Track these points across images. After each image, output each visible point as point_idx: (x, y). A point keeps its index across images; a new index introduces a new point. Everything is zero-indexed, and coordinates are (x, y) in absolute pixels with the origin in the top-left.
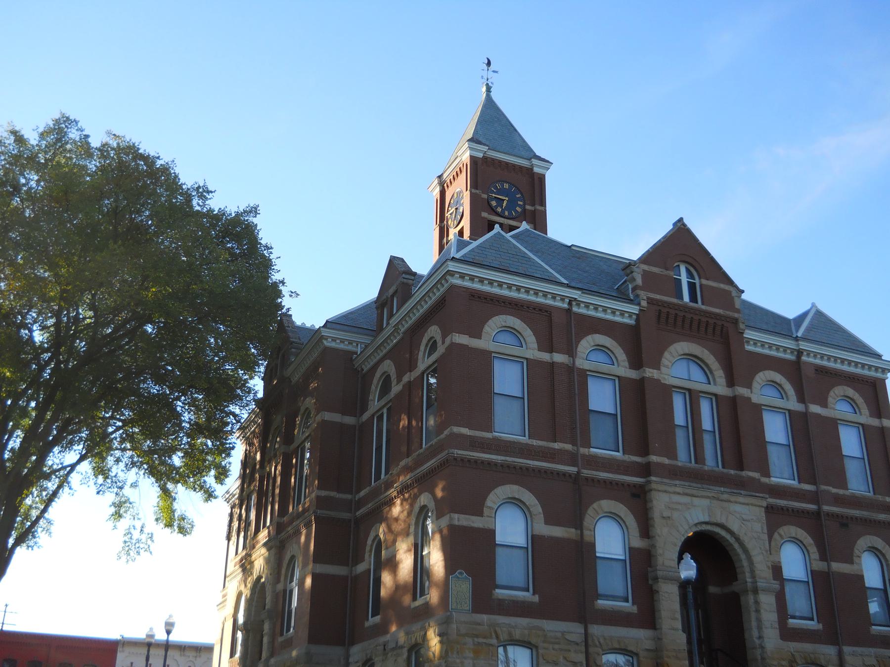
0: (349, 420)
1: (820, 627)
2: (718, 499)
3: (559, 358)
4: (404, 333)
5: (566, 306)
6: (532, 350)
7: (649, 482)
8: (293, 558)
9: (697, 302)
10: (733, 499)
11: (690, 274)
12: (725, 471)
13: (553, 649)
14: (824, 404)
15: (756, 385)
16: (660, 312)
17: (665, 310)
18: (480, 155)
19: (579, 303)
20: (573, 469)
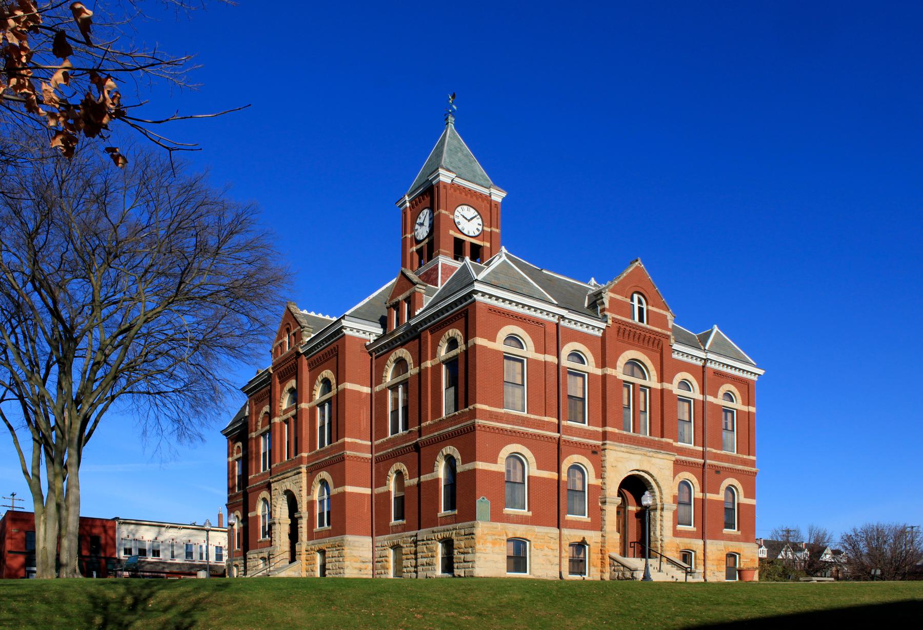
2: (646, 455)
9: (643, 322)
10: (655, 455)
12: (652, 438)
16: (619, 328)
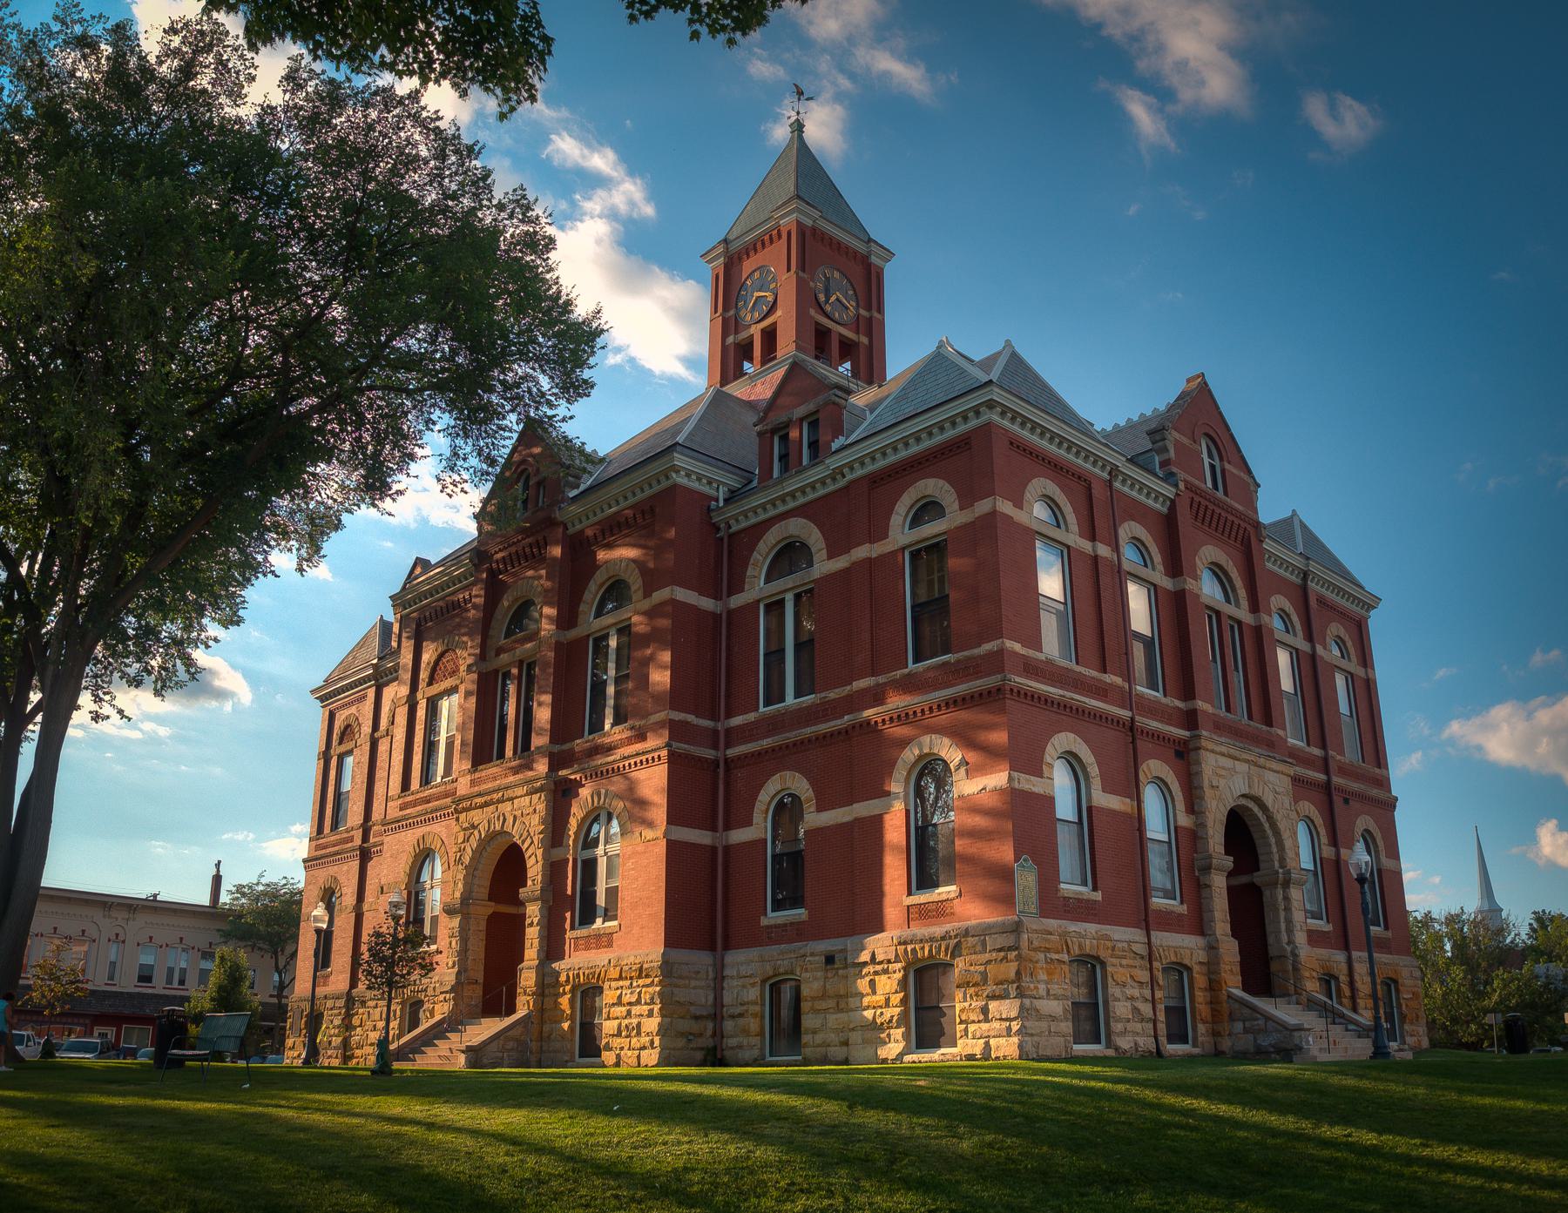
0: (707, 603)
2: (1256, 765)
7: (1199, 737)
13: (1121, 965)
20: (1125, 714)
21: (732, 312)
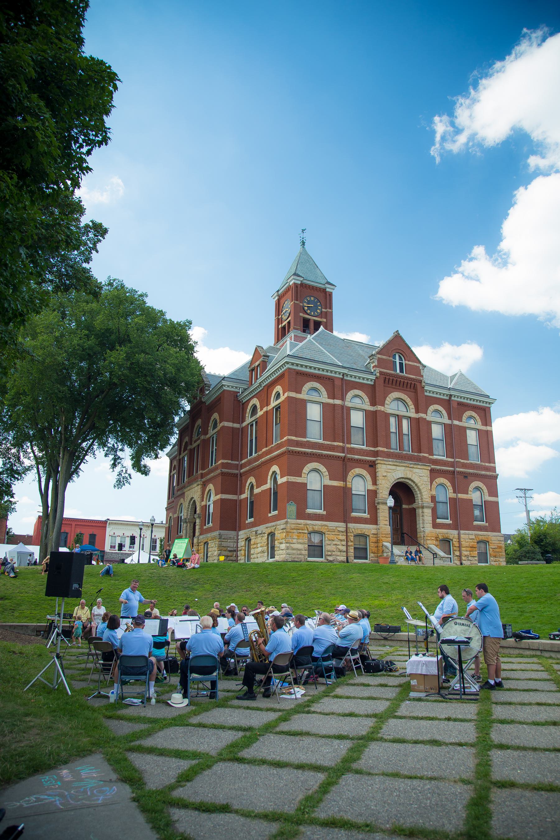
0: (236, 425)
1: (451, 522)
2: (408, 467)
3: (338, 402)
4: (264, 387)
5: (341, 376)
6: (324, 398)
8: (210, 490)
10: (415, 466)
11: (400, 359)
14: (460, 420)
15: (429, 412)
17: (388, 377)
18: (299, 282)
19: (347, 375)
20: (342, 455)
21: (280, 316)
